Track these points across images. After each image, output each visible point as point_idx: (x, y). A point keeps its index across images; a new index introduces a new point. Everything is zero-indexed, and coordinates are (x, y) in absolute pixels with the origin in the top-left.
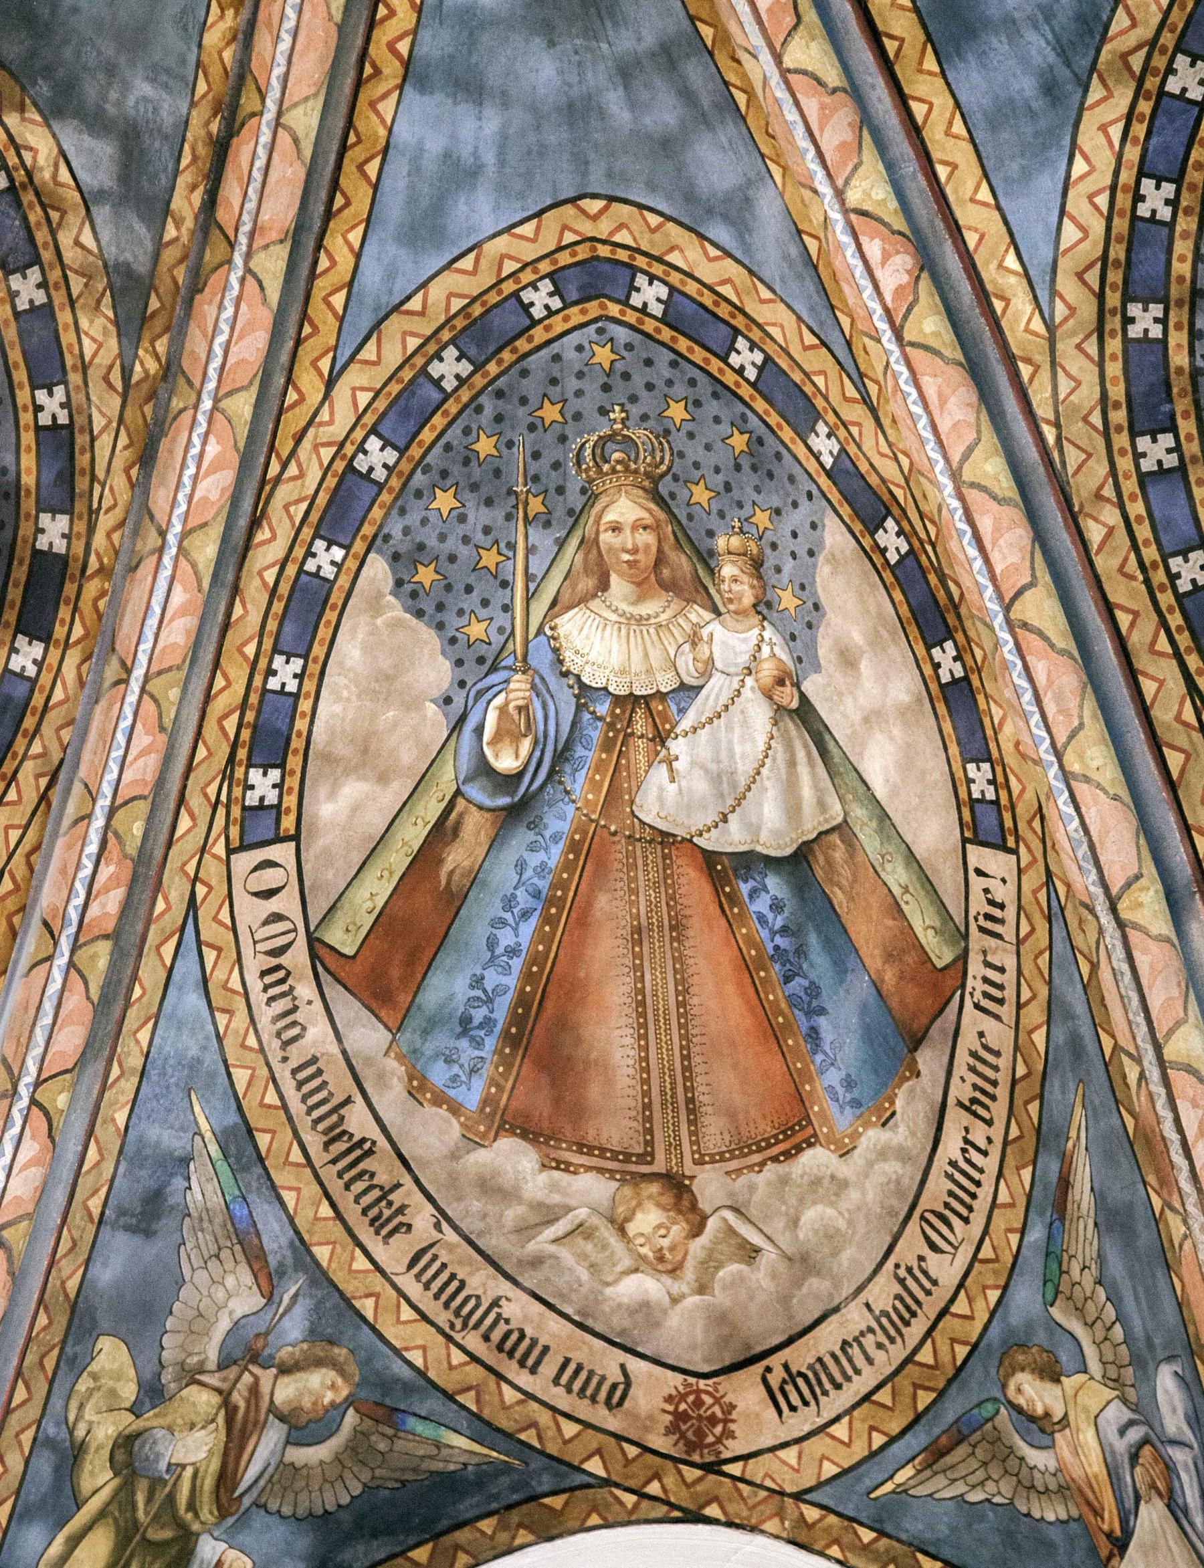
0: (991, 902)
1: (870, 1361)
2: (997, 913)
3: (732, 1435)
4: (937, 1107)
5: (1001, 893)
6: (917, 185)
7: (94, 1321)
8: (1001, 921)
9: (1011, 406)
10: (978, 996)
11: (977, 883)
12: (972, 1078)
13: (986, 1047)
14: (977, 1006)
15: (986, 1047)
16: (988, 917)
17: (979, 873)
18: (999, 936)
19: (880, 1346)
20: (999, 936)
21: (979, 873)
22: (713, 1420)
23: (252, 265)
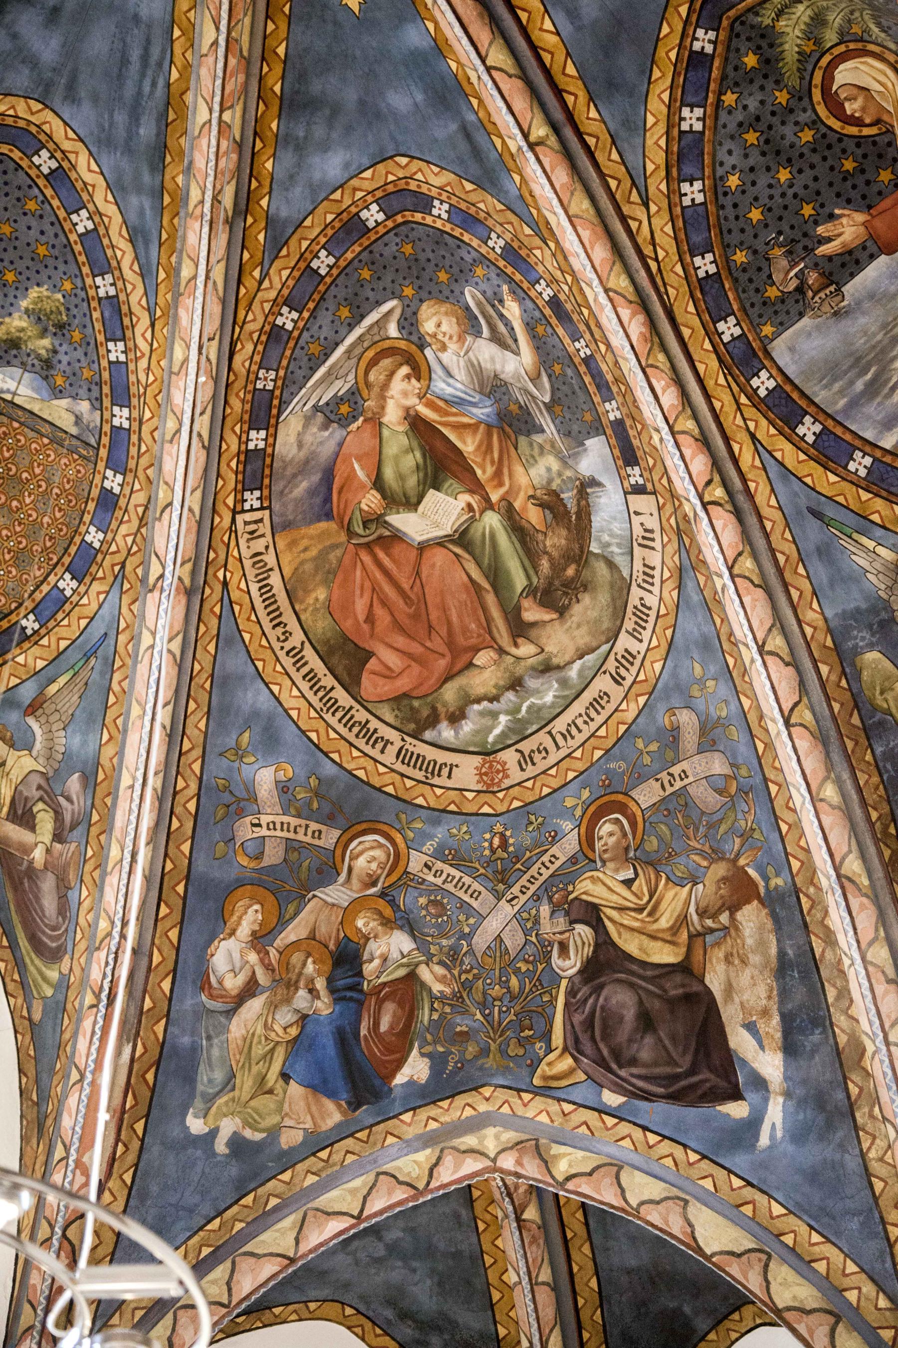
0: (646, 530)
1: (580, 731)
2: (648, 535)
3: (507, 777)
4: (596, 220)
5: (653, 523)
6: (564, 1268)
7: (296, 506)
8: (653, 540)
9: (752, 520)
10: (640, 581)
11: (636, 520)
12: (634, 619)
13: (643, 605)
14: (639, 586)
15: (643, 605)
16: (644, 538)
17: (637, 513)
18: (653, 548)
19: (585, 722)
20: (653, 548)
21: (637, 513)
22: (498, 772)
23: (488, 63)
